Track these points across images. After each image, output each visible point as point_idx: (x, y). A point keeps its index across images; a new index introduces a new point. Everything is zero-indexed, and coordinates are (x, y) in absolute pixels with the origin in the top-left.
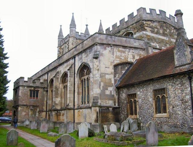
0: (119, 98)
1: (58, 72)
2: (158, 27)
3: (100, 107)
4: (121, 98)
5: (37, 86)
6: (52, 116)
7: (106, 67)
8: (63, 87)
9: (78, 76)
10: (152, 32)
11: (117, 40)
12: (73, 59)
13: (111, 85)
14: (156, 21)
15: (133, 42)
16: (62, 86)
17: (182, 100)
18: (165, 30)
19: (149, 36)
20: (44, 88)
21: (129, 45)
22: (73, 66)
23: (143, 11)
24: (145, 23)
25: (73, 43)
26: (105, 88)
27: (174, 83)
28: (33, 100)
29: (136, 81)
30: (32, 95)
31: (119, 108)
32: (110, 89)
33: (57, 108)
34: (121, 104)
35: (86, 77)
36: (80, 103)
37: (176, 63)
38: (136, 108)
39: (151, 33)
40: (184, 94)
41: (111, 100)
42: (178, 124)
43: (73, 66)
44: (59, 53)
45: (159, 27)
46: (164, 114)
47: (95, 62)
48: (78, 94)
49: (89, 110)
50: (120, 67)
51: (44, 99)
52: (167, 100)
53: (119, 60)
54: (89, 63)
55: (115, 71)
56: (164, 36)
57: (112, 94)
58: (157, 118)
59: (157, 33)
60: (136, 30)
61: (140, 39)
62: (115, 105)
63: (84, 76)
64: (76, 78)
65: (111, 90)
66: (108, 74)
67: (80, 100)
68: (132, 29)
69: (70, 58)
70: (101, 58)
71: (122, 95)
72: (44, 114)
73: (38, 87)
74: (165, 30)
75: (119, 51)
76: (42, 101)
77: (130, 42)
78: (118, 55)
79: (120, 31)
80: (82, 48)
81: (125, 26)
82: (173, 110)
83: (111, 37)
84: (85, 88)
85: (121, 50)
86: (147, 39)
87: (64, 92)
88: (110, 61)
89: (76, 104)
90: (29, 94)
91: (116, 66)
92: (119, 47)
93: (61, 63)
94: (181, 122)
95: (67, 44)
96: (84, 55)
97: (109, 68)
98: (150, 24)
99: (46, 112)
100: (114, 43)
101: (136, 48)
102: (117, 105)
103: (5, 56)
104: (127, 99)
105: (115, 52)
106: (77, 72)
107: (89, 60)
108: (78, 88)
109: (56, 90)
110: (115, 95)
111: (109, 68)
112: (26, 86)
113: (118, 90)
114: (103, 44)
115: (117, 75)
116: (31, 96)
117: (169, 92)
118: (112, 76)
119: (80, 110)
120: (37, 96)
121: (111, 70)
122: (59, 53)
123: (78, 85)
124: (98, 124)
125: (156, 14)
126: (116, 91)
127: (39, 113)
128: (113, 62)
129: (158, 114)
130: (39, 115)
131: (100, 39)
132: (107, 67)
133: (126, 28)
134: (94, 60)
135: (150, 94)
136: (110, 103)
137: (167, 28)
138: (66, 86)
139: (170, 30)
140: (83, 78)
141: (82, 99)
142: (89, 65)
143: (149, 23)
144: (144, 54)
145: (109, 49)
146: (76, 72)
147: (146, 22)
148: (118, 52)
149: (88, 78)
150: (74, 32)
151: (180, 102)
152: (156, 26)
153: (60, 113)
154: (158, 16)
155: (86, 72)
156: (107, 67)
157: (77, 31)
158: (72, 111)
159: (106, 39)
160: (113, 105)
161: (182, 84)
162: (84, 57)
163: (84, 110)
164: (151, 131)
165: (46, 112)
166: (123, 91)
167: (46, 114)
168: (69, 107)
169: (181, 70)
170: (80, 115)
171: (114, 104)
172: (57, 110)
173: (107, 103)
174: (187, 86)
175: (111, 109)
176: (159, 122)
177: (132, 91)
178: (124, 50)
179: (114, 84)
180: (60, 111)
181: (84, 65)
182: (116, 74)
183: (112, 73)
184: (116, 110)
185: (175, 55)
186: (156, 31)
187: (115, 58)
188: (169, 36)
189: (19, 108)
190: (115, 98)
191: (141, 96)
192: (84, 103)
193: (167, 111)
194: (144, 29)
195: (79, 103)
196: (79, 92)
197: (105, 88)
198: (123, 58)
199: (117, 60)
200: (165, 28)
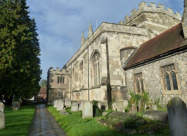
0: (126, 78)
1: (78, 62)
4: (128, 78)
7: (113, 51)
10: (153, 22)
11: (122, 28)
13: (118, 67)
14: (156, 13)
15: (136, 30)
19: (151, 25)
23: (144, 4)
24: (146, 14)
32: (118, 70)
34: (128, 84)
35: (97, 62)
38: (142, 86)
41: (119, 80)
50: (125, 51)
53: (80, 71)
56: (164, 25)
57: (120, 74)
59: (157, 22)
62: (123, 84)
66: (115, 57)
69: (85, 49)
75: (124, 37)
76: (68, 85)
77: (133, 29)
92: (124, 34)
96: (94, 43)
102: (124, 85)
104: (134, 79)
108: (92, 72)
114: (110, 32)
115: (124, 58)
120: (63, 82)
121: (118, 53)
128: (120, 47)
131: (107, 27)
132: (114, 51)
137: (166, 18)
140: (95, 63)
143: (150, 14)
145: (115, 35)
148: (123, 39)
149: (98, 63)
152: (157, 17)
155: (97, 58)
156: (114, 51)
158: (88, 91)
159: (112, 27)
163: (96, 89)
168: (85, 88)
171: (121, 83)
172: (77, 91)
175: (119, 88)
177: (138, 70)
178: (128, 36)
179: (120, 66)
183: (118, 56)
184: (124, 89)
187: (121, 43)
188: (168, 25)
190: (123, 78)
191: (147, 74)
193: (179, 87)
194: (146, 19)
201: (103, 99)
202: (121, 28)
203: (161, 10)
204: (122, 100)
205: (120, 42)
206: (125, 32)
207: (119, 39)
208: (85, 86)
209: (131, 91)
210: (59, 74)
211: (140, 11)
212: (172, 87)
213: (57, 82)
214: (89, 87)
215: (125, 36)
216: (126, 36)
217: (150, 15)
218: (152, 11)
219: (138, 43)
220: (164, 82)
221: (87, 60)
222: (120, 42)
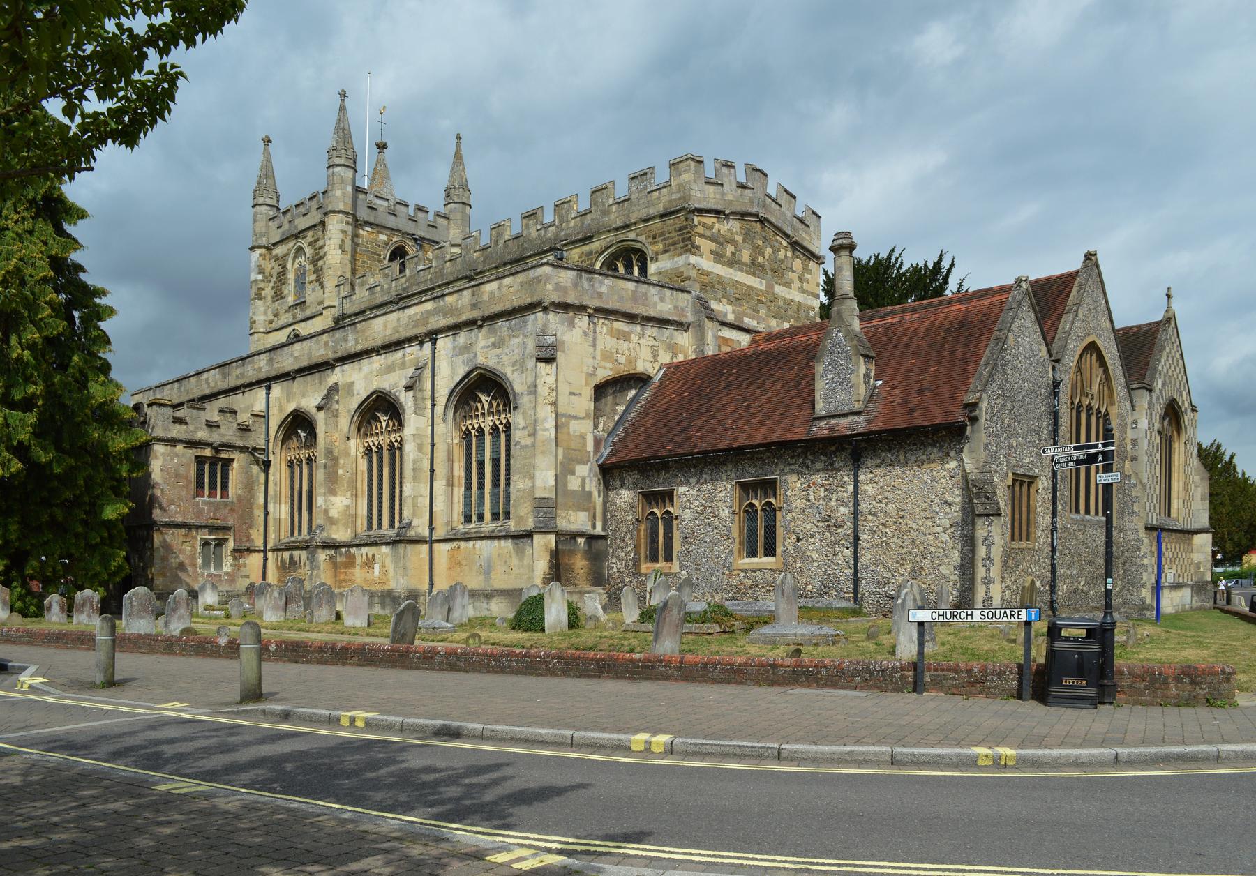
4: (615, 504)
5: (224, 440)
7: (572, 393)
8: (361, 450)
10: (718, 257)
12: (422, 343)
15: (656, 299)
18: (758, 250)
19: (707, 274)
20: (255, 449)
27: (808, 467)
28: (210, 503)
30: (206, 480)
31: (604, 537)
36: (458, 517)
37: (821, 407)
42: (810, 587)
43: (427, 373)
45: (739, 238)
48: (450, 483)
51: (253, 496)
53: (610, 365)
56: (754, 274)
58: (743, 571)
59: (733, 262)
60: (661, 246)
61: (675, 283)
62: (594, 527)
64: (438, 420)
65: (585, 476)
66: (575, 418)
69: (410, 340)
70: (560, 356)
72: (255, 560)
74: (758, 250)
75: (612, 332)
76: (246, 503)
79: (591, 237)
80: (474, 306)
81: (612, 216)
83: (590, 280)
84: (481, 464)
85: (618, 330)
86: (698, 286)
87: (366, 475)
88: (585, 369)
91: (601, 390)
93: (353, 350)
94: (817, 582)
99: (264, 551)
101: (662, 322)
102: (599, 530)
103: (97, 300)
108: (450, 459)
109: (329, 463)
110: (596, 494)
112: (180, 441)
115: (601, 420)
116: (200, 484)
117: (789, 493)
118: (589, 424)
119: (462, 544)
120: (225, 487)
121: (586, 403)
127: (235, 559)
128: (594, 374)
129: (747, 560)
130: (237, 566)
131: (558, 287)
134: (542, 365)
135: (723, 494)
137: (765, 239)
138: (396, 449)
143: (708, 220)
145: (582, 322)
146: (441, 400)
147: (701, 219)
148: (608, 338)
153: (353, 557)
157: (96, 152)
158: (425, 547)
159: (576, 285)
160: (588, 528)
162: (483, 348)
163: (479, 544)
166: (623, 480)
168: (412, 533)
169: (832, 429)
170: (464, 562)
172: (335, 546)
173: (572, 519)
174: (846, 478)
176: (749, 583)
180: (353, 550)
183: (588, 416)
185: (817, 378)
187: (598, 358)
192: (474, 518)
193: (779, 551)
198: (622, 359)
200: (760, 242)
202: (604, 289)
204: (588, 587)
206: (616, 306)
207: (594, 339)
208: (415, 523)
211: (675, 197)
212: (761, 550)
213: (193, 486)
214: (432, 529)
216: (620, 325)
217: (711, 227)
218: (720, 207)
219: (655, 355)
220: (741, 531)
221: (424, 399)
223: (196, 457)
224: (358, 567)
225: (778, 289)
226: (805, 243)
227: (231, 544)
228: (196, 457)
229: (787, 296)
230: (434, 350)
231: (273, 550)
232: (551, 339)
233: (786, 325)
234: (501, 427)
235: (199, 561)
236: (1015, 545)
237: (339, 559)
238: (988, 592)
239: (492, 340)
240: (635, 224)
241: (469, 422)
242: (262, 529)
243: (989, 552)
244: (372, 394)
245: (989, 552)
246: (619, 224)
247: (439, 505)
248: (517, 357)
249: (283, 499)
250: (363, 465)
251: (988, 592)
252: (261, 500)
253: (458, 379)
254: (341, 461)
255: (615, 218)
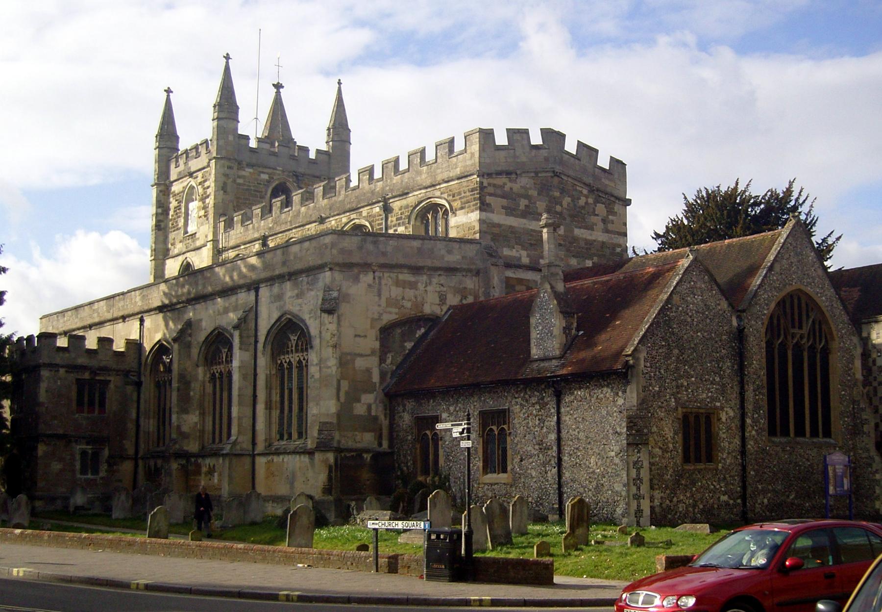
2: (531, 192)
3: (338, 450)
5: (103, 364)
6: (169, 474)
7: (356, 336)
9: (269, 348)
10: (510, 211)
12: (249, 290)
13: (369, 388)
15: (443, 252)
16: (205, 375)
17: (540, 443)
19: (499, 225)
20: (129, 371)
21: (429, 263)
22: (252, 315)
25: (225, 184)
26: (353, 397)
27: (527, 401)
29: (438, 384)
31: (392, 453)
32: (368, 398)
33: (185, 448)
35: (294, 358)
37: (535, 352)
39: (504, 216)
40: (545, 430)
41: (370, 431)
42: (530, 499)
44: (160, 211)
46: (501, 475)
47: (327, 322)
48: (269, 406)
49: (305, 459)
50: (399, 331)
52: (508, 439)
54: (306, 317)
55: (382, 345)
57: (373, 413)
62: (380, 445)
63: (288, 353)
64: (259, 354)
65: (369, 403)
66: (361, 355)
67: (275, 428)
68: (445, 196)
70: (344, 308)
71: (401, 417)
72: (127, 467)
73: (105, 369)
75: (398, 283)
78: (393, 295)
79: (407, 193)
80: (284, 263)
81: (424, 176)
82: (520, 467)
84: (290, 391)
85: (404, 282)
89: (261, 437)
90: (74, 395)
91: (386, 332)
95: (200, 179)
97: (366, 336)
98: (505, 184)
100: (382, 260)
101: (450, 270)
104: (415, 431)
105: (384, 287)
106: (266, 338)
107: (306, 309)
108: (269, 388)
110: (382, 417)
111: (366, 336)
113: (391, 402)
115: (390, 356)
116: (80, 403)
117: (516, 421)
118: (373, 363)
120: (102, 404)
121: (372, 343)
122: (160, 211)
123: (267, 381)
124: (331, 498)
125: (527, 149)
126: (385, 406)
127: (110, 465)
128: (380, 319)
129: (489, 475)
132: (359, 336)
133: (426, 188)
134: (325, 315)
136: (367, 439)
137: (563, 191)
139: (575, 199)
140: (286, 358)
141: (281, 424)
142: (306, 325)
143: (500, 181)
144: (477, 288)
145: (367, 278)
146: (262, 338)
147: (491, 181)
148: (393, 288)
149: (300, 362)
150: (231, 138)
151: (537, 447)
153: (199, 466)
154: (534, 152)
156: (359, 336)
159: (360, 248)
160: (375, 445)
161: (543, 406)
163: (287, 458)
164: (438, 506)
165: (136, 459)
166: (404, 406)
167: (136, 466)
170: (276, 473)
171: (376, 443)
173: (358, 438)
174: (553, 411)
175: (367, 457)
180: (200, 460)
181: (290, 320)
182: (386, 354)
183: (373, 352)
185: (532, 329)
186: (522, 207)
187: (384, 304)
189: (41, 449)
192: (286, 437)
193: (509, 468)
195: (270, 435)
196: (271, 401)
197: (353, 397)
199: (390, 313)
201: (320, 490)
202: (389, 249)
203: (546, 159)
205: (383, 299)
206: (402, 261)
209: (405, 468)
210: (83, 368)
212: (703, 457)
213: (74, 405)
215: (401, 277)
217: (502, 187)
222: (383, 299)
223: (78, 380)
224: (203, 475)
225: (578, 232)
226: (609, 190)
227: (106, 452)
228: (78, 380)
229: (589, 238)
230: (257, 296)
231: (142, 458)
232: (335, 294)
233: (589, 263)
234: (285, 365)
235: (78, 466)
236: (689, 467)
237: (190, 468)
238: (639, 506)
239: (296, 291)
240: (440, 184)
241: (282, 357)
242: (134, 440)
243: (638, 474)
244: (214, 330)
245: (638, 474)
246: (428, 183)
247: (260, 425)
248: (312, 307)
249: (152, 414)
250: (209, 388)
251: (639, 506)
252: (134, 415)
253: (273, 322)
254: (193, 385)
255: (424, 178)
